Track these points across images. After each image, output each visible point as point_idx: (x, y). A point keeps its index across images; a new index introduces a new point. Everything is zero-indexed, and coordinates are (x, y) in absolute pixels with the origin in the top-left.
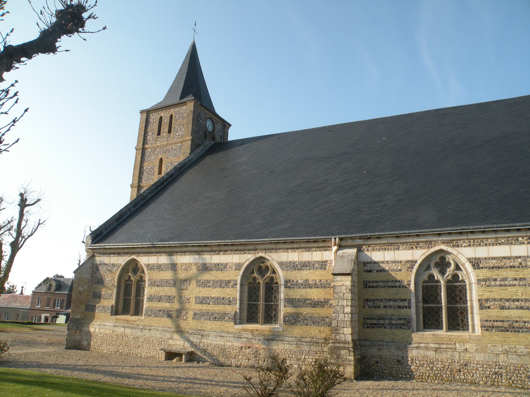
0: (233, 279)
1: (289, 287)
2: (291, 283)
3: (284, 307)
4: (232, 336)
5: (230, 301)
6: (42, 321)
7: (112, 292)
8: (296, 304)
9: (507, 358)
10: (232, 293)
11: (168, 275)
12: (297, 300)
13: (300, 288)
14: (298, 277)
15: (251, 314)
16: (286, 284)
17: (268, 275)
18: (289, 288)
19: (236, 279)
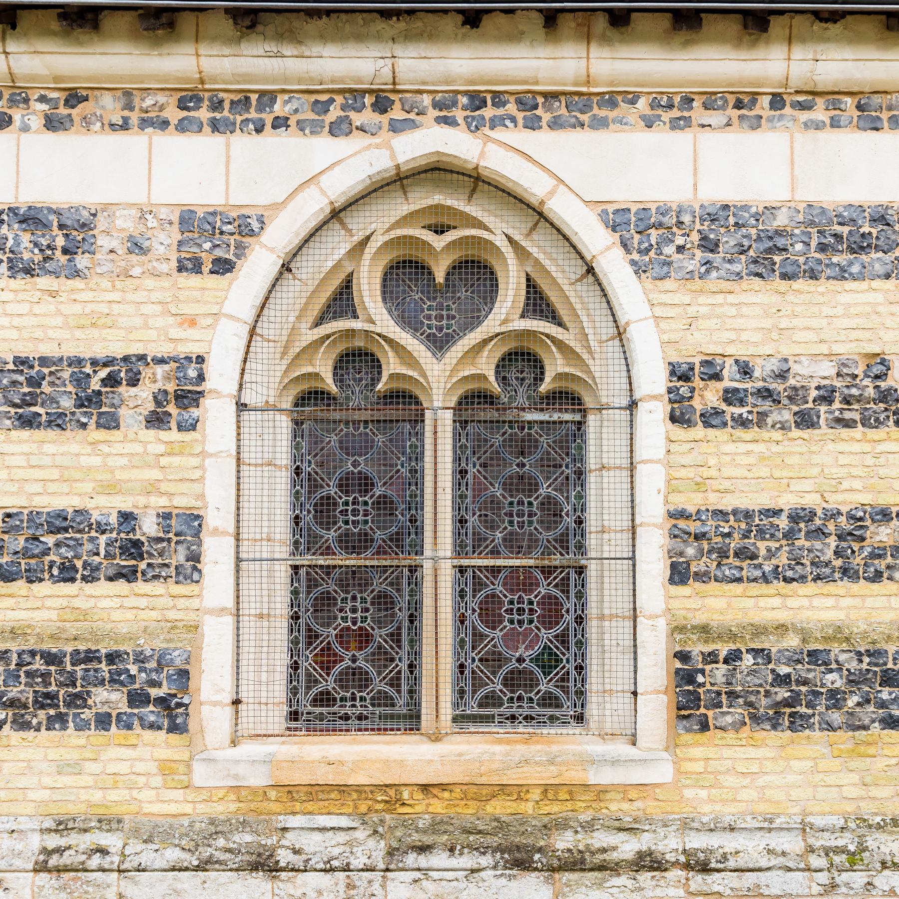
0: (163, 349)
1: (711, 419)
2: (730, 379)
3: (672, 581)
4: (173, 855)
5: (137, 544)
6: (254, 97)
7: (459, 96)
8: (783, 559)
9: (265, 461)
10: (155, 474)
11: (182, 295)
12: (783, 523)
13: (806, 421)
14: (799, 336)
15: (327, 659)
16: (684, 391)
17: (491, 324)
18: (707, 425)
19: (194, 349)
